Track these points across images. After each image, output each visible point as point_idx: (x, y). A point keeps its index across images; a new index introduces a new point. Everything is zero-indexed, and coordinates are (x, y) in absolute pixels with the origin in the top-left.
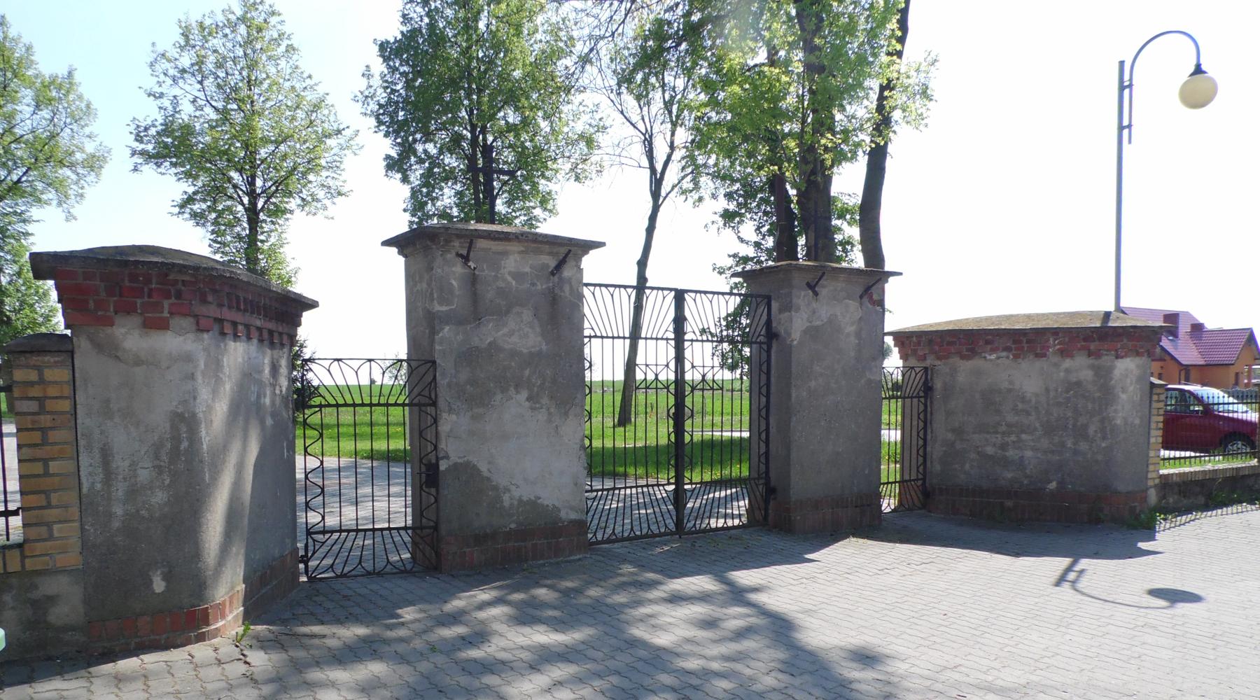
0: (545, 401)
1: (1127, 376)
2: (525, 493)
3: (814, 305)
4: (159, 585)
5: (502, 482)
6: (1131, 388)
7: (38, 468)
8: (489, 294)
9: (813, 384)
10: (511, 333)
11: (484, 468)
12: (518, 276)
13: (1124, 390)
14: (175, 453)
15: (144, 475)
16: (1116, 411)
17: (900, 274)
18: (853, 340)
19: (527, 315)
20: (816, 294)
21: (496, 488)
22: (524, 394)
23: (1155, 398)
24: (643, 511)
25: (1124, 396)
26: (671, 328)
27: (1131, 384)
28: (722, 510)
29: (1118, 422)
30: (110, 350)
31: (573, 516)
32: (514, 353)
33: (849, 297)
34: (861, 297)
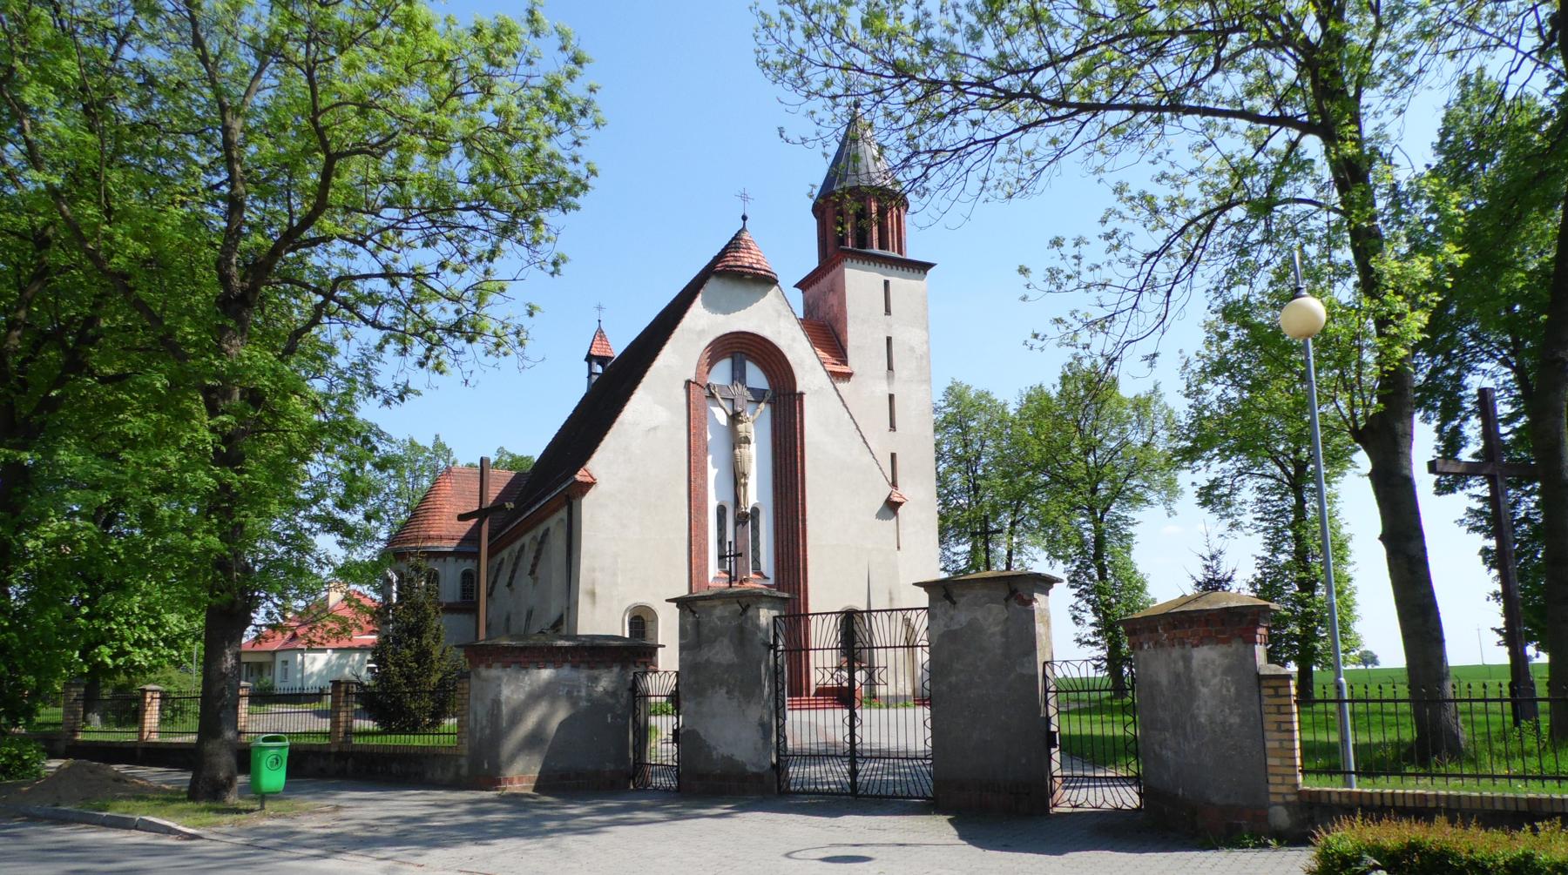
0: (736, 694)
1: (1206, 666)
2: (723, 750)
3: (952, 612)
4: (486, 766)
5: (712, 743)
6: (1216, 681)
7: (1286, 744)
8: (705, 631)
9: (953, 679)
10: (717, 653)
11: (702, 734)
12: (721, 619)
13: (1205, 683)
14: (492, 715)
15: (484, 723)
16: (1198, 708)
17: (915, 584)
18: (999, 639)
19: (726, 641)
20: (954, 603)
21: (708, 746)
22: (723, 691)
23: (1265, 692)
24: (891, 778)
25: (1205, 690)
26: (925, 637)
27: (1214, 675)
28: (897, 778)
29: (1203, 720)
30: (478, 676)
31: (754, 770)
32: (719, 665)
33: (992, 601)
34: (1007, 600)
